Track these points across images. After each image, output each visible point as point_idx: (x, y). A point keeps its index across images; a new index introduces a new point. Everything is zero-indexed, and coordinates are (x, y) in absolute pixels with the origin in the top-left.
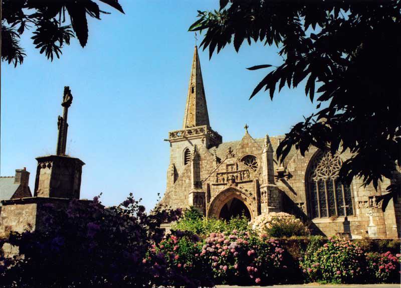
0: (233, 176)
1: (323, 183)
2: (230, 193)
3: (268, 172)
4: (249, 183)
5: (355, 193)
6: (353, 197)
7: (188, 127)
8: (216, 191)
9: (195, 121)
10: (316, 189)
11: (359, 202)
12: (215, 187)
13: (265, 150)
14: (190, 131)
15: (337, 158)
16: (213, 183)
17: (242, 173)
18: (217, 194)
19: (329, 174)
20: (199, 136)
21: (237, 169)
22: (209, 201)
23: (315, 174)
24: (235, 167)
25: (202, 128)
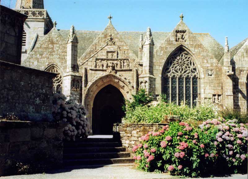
0: (113, 63)
1: (176, 79)
2: (108, 79)
3: (150, 64)
4: (129, 72)
5: (202, 91)
6: (200, 94)
7: (23, 8)
8: (94, 77)
9: (32, 3)
10: (169, 84)
11: (205, 98)
12: (93, 72)
13: (70, 40)
14: (27, 12)
15: (189, 58)
16: (91, 68)
17: (122, 62)
18: (95, 79)
19: (181, 72)
20: (37, 19)
21: (117, 57)
22: (86, 86)
23: (169, 70)
24: (115, 54)
25: (41, 12)
